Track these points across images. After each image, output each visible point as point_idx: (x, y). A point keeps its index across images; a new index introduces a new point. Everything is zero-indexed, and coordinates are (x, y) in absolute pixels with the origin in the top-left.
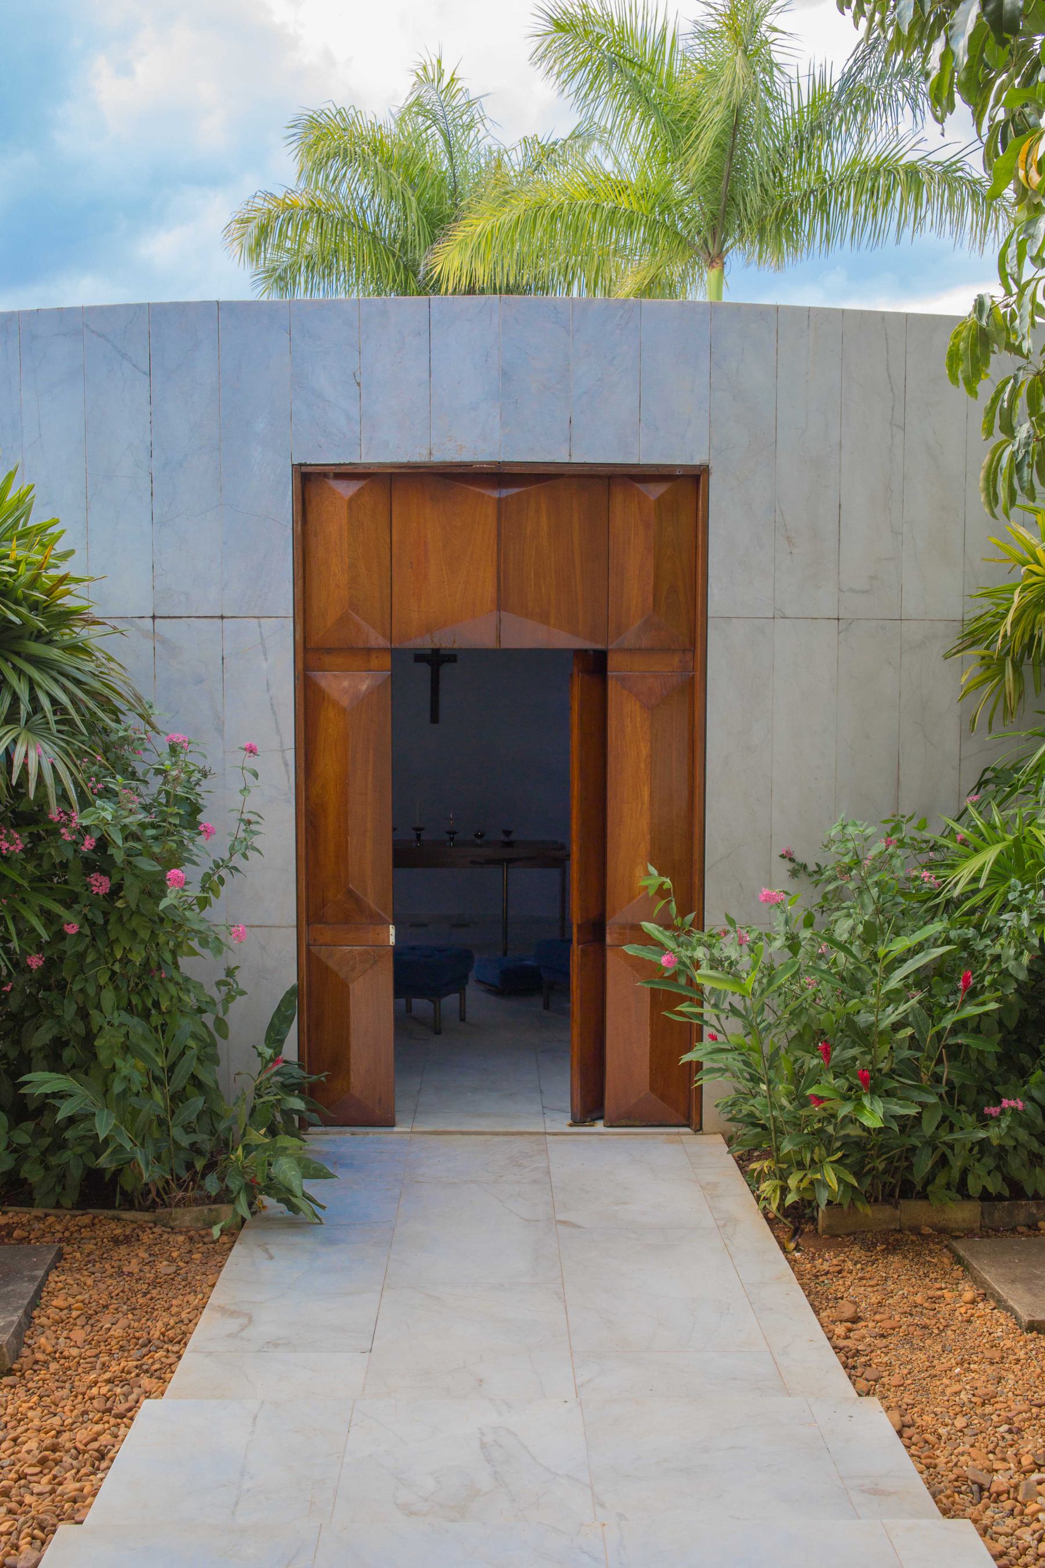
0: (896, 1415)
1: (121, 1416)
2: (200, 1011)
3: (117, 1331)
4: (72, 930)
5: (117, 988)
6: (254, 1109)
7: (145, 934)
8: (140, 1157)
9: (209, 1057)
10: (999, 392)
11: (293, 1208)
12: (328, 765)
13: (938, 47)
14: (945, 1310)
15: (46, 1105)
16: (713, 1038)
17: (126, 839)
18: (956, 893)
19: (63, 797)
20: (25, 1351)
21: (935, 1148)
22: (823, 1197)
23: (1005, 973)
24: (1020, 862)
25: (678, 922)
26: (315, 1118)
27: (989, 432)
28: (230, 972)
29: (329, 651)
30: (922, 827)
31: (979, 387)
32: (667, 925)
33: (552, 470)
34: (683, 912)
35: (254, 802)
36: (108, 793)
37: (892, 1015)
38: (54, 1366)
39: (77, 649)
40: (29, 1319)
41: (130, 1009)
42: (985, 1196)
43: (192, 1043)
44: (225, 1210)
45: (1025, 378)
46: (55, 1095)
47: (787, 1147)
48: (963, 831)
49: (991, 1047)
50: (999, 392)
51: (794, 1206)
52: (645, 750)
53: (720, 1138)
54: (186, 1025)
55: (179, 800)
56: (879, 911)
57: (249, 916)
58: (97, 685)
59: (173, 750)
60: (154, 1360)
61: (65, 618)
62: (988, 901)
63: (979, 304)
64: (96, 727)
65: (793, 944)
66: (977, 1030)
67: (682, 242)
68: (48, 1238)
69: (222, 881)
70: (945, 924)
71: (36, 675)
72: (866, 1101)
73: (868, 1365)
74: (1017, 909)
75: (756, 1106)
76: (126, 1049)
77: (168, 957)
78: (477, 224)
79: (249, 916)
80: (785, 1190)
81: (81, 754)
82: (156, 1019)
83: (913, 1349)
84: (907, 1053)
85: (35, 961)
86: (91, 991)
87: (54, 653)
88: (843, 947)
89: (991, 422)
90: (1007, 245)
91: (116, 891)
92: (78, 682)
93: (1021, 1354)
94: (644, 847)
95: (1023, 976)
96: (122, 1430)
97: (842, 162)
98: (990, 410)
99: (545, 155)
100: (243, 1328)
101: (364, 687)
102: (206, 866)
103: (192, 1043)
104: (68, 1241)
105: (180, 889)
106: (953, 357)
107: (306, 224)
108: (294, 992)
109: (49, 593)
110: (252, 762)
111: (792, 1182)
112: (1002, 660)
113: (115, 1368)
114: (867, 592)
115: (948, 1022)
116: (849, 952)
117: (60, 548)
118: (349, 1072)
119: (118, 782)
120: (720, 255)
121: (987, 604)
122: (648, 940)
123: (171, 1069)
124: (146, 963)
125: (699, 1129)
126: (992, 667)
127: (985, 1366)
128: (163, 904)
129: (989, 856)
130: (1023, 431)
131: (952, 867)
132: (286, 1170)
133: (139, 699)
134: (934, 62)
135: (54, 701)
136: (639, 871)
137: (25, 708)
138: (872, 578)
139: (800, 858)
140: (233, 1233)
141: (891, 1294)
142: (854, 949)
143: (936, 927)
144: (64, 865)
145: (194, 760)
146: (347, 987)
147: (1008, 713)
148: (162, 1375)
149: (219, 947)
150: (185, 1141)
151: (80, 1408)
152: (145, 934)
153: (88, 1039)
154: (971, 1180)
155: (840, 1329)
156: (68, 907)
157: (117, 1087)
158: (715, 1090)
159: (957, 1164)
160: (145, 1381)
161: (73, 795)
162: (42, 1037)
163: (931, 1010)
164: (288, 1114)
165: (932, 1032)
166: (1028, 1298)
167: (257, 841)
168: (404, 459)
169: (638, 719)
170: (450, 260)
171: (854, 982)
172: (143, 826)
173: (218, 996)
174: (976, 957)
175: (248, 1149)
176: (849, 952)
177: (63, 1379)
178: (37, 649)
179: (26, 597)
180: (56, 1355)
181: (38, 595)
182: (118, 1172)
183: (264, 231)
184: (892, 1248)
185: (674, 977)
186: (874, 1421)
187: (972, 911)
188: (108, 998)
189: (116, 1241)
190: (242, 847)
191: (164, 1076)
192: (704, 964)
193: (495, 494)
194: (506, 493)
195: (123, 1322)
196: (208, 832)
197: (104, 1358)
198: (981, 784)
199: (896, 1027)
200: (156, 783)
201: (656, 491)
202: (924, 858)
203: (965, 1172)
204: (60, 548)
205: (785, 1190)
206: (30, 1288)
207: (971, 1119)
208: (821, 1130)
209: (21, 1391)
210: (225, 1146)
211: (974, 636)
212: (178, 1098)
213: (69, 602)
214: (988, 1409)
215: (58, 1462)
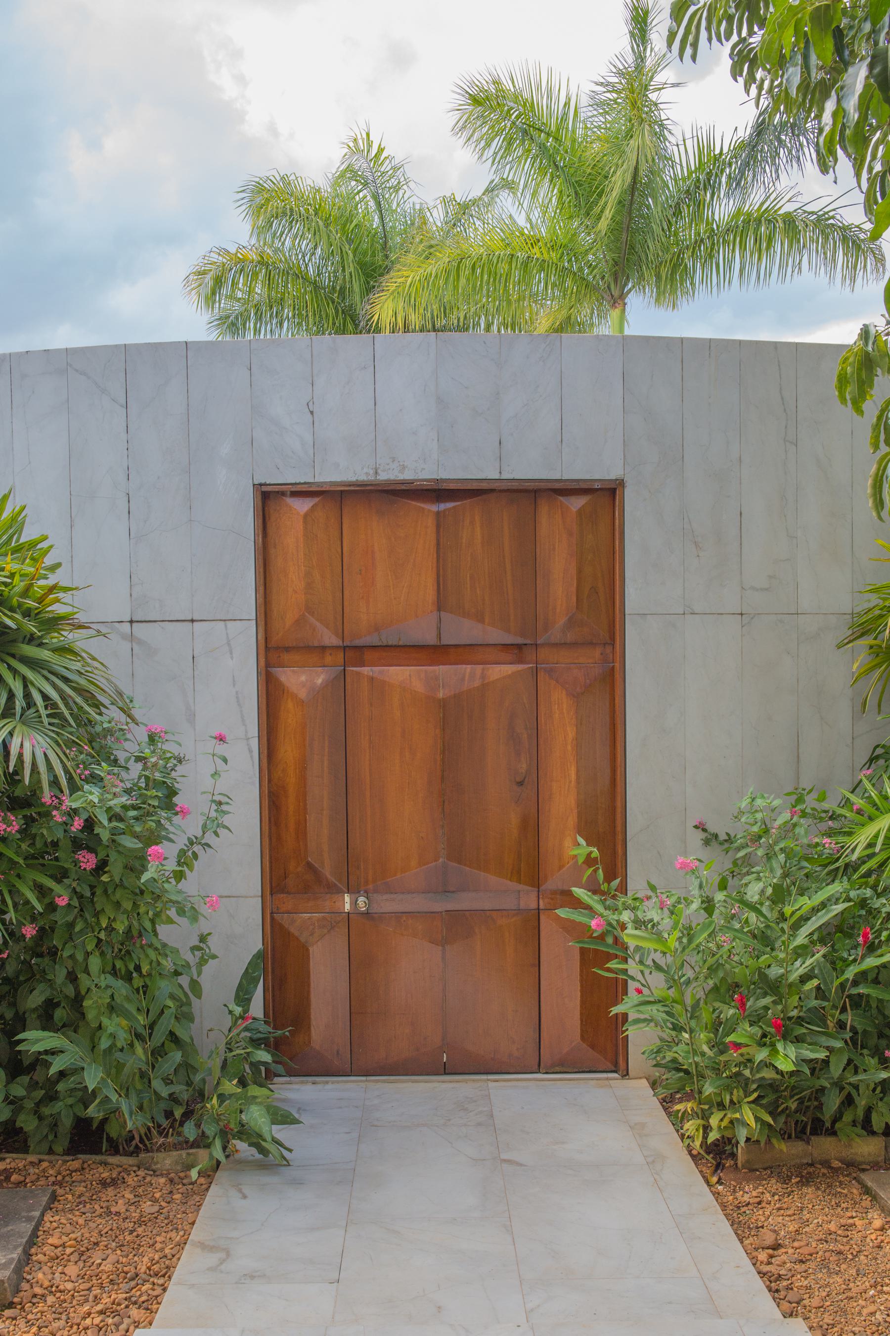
2: (177, 973)
3: (107, 1267)
4: (62, 902)
5: (102, 954)
7: (127, 905)
8: (125, 1108)
9: (185, 1015)
12: (288, 752)
13: (830, 106)
14: (857, 1237)
15: (40, 1061)
16: (639, 991)
18: (854, 857)
20: (25, 1286)
21: (842, 1089)
22: (742, 1134)
26: (280, 1069)
27: (876, 447)
28: (203, 939)
29: (288, 649)
30: (822, 798)
33: (484, 486)
34: (610, 877)
36: (94, 779)
37: (800, 968)
38: (50, 1299)
41: (114, 972)
43: (170, 1003)
46: (46, 1052)
47: (709, 1089)
51: (716, 1143)
52: (571, 733)
54: (164, 987)
59: (152, 739)
64: (83, 723)
65: (708, 906)
66: (876, 981)
69: (195, 856)
71: (29, 674)
72: (780, 1046)
73: (789, 1288)
75: (680, 1052)
76: (112, 1008)
77: (148, 925)
80: (707, 1129)
82: (137, 982)
83: (830, 1274)
84: (814, 1003)
85: (29, 931)
86: (80, 957)
87: (44, 654)
89: (877, 437)
91: (101, 867)
92: (66, 680)
94: (572, 821)
102: (182, 842)
103: (170, 1003)
104: (60, 1184)
106: (843, 381)
107: (255, 274)
108: (260, 956)
110: (221, 749)
111: (714, 1121)
113: (106, 1300)
114: (766, 589)
115: (851, 973)
117: (48, 561)
118: (309, 1028)
120: (622, 296)
122: (578, 904)
123: (152, 1026)
124: (128, 931)
125: (626, 1074)
128: (145, 877)
135: (45, 697)
136: (568, 842)
137: (19, 703)
138: (770, 577)
139: (712, 828)
141: (807, 1223)
142: (764, 910)
144: (55, 844)
146: (308, 950)
148: (150, 1305)
149: (195, 916)
150: (165, 1092)
152: (127, 905)
153: (77, 1001)
154: (874, 1117)
155: (763, 1256)
156: (59, 881)
157: (104, 1044)
158: (641, 1039)
159: (862, 1103)
160: (134, 1312)
161: (64, 782)
162: (35, 999)
163: (835, 963)
164: (255, 1066)
165: (836, 983)
167: (226, 820)
168: (352, 478)
169: (565, 706)
171: (764, 939)
172: (125, 808)
175: (222, 1098)
176: (759, 912)
178: (29, 650)
179: (20, 605)
180: (52, 1289)
181: (30, 603)
182: (105, 1121)
183: (219, 282)
184: (806, 1180)
185: (602, 937)
187: (868, 874)
188: (95, 963)
189: (104, 1184)
191: (145, 1033)
192: (630, 926)
193: (434, 508)
194: (443, 506)
195: (112, 1258)
197: (96, 1291)
198: (872, 760)
200: (136, 769)
201: (577, 503)
203: (869, 1111)
204: (48, 561)
205: (707, 1129)
206: (28, 1228)
207: (873, 1062)
208: (738, 1074)
209: (22, 1323)
213: (59, 609)
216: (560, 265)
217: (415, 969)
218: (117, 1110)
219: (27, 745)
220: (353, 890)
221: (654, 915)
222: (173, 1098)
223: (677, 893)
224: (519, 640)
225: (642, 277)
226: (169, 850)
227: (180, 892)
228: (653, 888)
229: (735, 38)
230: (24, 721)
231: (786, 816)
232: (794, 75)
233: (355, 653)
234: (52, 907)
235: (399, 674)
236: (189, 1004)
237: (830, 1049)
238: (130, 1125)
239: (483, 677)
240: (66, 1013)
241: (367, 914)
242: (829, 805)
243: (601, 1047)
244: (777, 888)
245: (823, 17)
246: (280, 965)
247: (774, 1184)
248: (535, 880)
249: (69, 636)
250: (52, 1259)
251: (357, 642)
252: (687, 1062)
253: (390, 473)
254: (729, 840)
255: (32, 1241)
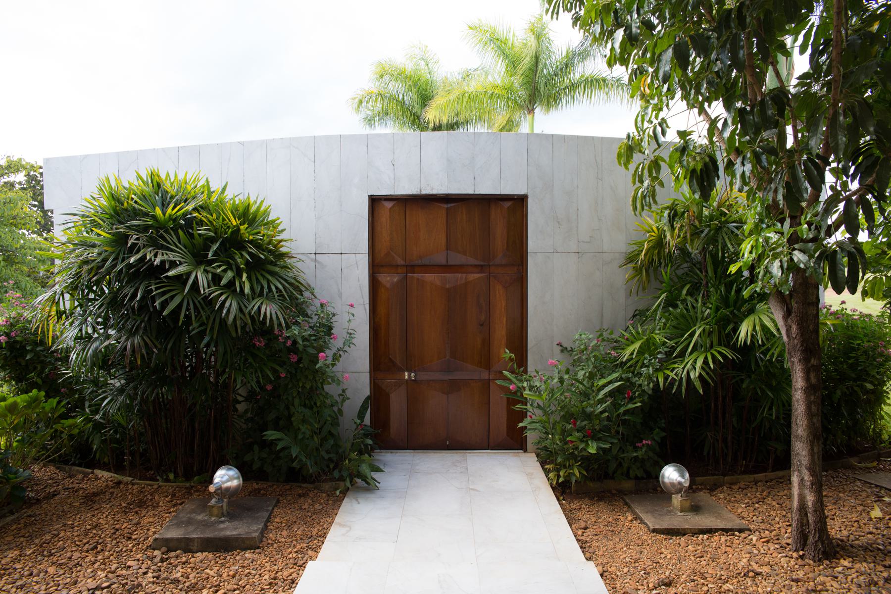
0: (600, 568)
1: (301, 566)
2: (332, 406)
3: (299, 532)
4: (283, 375)
5: (300, 398)
6: (353, 444)
7: (311, 377)
8: (308, 463)
9: (335, 423)
10: (637, 168)
11: (367, 483)
12: (382, 310)
13: (609, 45)
14: (620, 524)
15: (273, 443)
16: (531, 417)
17: (303, 341)
18: (624, 360)
19: (280, 324)
20: (265, 539)
21: (617, 460)
22: (573, 480)
23: (643, 391)
24: (649, 347)
25: (517, 371)
26: (377, 446)
27: (634, 183)
28: (344, 391)
29: (382, 266)
30: (611, 333)
31: (629, 166)
32: (512, 372)
34: (519, 367)
35: (352, 325)
36: (296, 323)
37: (600, 408)
38: (275, 546)
39: (285, 267)
40: (266, 526)
41: (305, 406)
42: (636, 478)
43: (329, 419)
44: (342, 484)
45: (647, 163)
46: (276, 440)
47: (559, 460)
48: (627, 335)
49: (638, 420)
50: (637, 168)
51: (562, 482)
52: (504, 304)
53: (534, 455)
54: (327, 412)
55: (324, 326)
56: (595, 367)
57: (352, 365)
58: (293, 281)
59: (322, 306)
60: (313, 543)
61: (282, 255)
62: (637, 362)
63: (628, 136)
64: (294, 296)
65: (561, 381)
66: (633, 413)
67: (520, 106)
68: (274, 494)
69: (340, 356)
70: (621, 371)
71: (270, 278)
72: (590, 442)
73: (590, 547)
74: (648, 366)
75: (547, 443)
76: (304, 421)
77: (320, 385)
78: (439, 101)
79: (352, 365)
80: (559, 476)
81: (287, 308)
82: (315, 409)
83: (608, 540)
84: (606, 423)
85: (269, 387)
86: (290, 399)
87: (277, 269)
88: (581, 383)
89: (635, 179)
90: (637, 116)
91: (300, 361)
92: (286, 280)
93: (650, 542)
94: (504, 341)
95: (650, 392)
96: (301, 572)
97: (577, 76)
98: (634, 175)
99: (467, 76)
100: (348, 531)
101: (395, 280)
102: (334, 350)
103: (329, 419)
104: (281, 495)
105: (325, 358)
106: (619, 156)
107: (376, 99)
108: (368, 398)
109: (275, 246)
110: (352, 310)
111: (561, 473)
112: (641, 268)
113: (298, 547)
115: (622, 410)
116: (583, 385)
117: (280, 228)
119: (300, 319)
120: (533, 110)
121: (635, 247)
122: (505, 378)
123: (321, 428)
124: (311, 388)
125: (526, 451)
126: (638, 271)
127: (636, 547)
128: (317, 366)
129: (637, 345)
130: (646, 184)
131: (623, 349)
132: (364, 468)
133: (309, 286)
134: (608, 52)
135: (277, 288)
136: (502, 350)
137: (266, 290)
139: (565, 345)
140: (344, 493)
141: (600, 518)
142: (585, 383)
143: (615, 375)
144: (280, 351)
145: (329, 309)
147: (644, 289)
148: (317, 549)
149: (339, 383)
150: (326, 456)
151: (285, 563)
152: (311, 377)
153: (290, 416)
154: (631, 472)
155: (580, 532)
156: (281, 367)
157: (300, 436)
158: (532, 437)
159: (625, 465)
160: (310, 552)
161: (284, 324)
162: (272, 416)
163: (615, 406)
164: (366, 445)
165: (616, 414)
166: (653, 519)
167: (354, 341)
168: (410, 193)
170: (431, 114)
171: (585, 395)
172: (310, 335)
173: (339, 400)
174: (633, 384)
175: (350, 460)
176: (583, 385)
177: (279, 551)
178: (271, 268)
179: (267, 248)
180: (276, 541)
181: (271, 247)
182: (300, 469)
183: (361, 102)
184: (600, 499)
185: (515, 393)
186: (592, 571)
187: (631, 366)
188: (297, 402)
189: (300, 496)
190: (349, 342)
191: (318, 432)
192: (527, 389)
193: (446, 206)
194: (449, 205)
195: (302, 529)
196: (335, 338)
197: (295, 543)
198: (634, 316)
199: (602, 413)
200: (315, 318)
201: (507, 204)
202: (612, 345)
203: (629, 469)
204: (280, 228)
205: (559, 476)
206: (266, 515)
207: (631, 448)
208: (573, 453)
209: (263, 555)
210: (342, 458)
211: (631, 258)
212: (324, 440)
213: (283, 250)
214: (637, 564)
215: (276, 584)
216: (507, 96)
217: (436, 404)
218: (305, 464)
219: (268, 309)
220: (410, 371)
221: (538, 384)
222: (330, 460)
223: (548, 374)
224: (482, 263)
225: (541, 101)
226: (329, 353)
227: (333, 372)
228: (537, 372)
229: (573, 11)
230: (268, 298)
231: (595, 342)
232: (597, 29)
233: (411, 268)
234: (279, 377)
235: (429, 277)
236: (338, 418)
237: (612, 443)
238: (311, 471)
239: (466, 278)
240: (285, 424)
241: (415, 380)
242: (615, 336)
243: (513, 440)
244: (590, 373)
245: (607, 8)
246: (377, 399)
247: (587, 501)
248: (487, 366)
249: (289, 261)
250: (276, 528)
251: (412, 263)
252: (552, 447)
253: (427, 191)
254: (572, 350)
255: (268, 520)
